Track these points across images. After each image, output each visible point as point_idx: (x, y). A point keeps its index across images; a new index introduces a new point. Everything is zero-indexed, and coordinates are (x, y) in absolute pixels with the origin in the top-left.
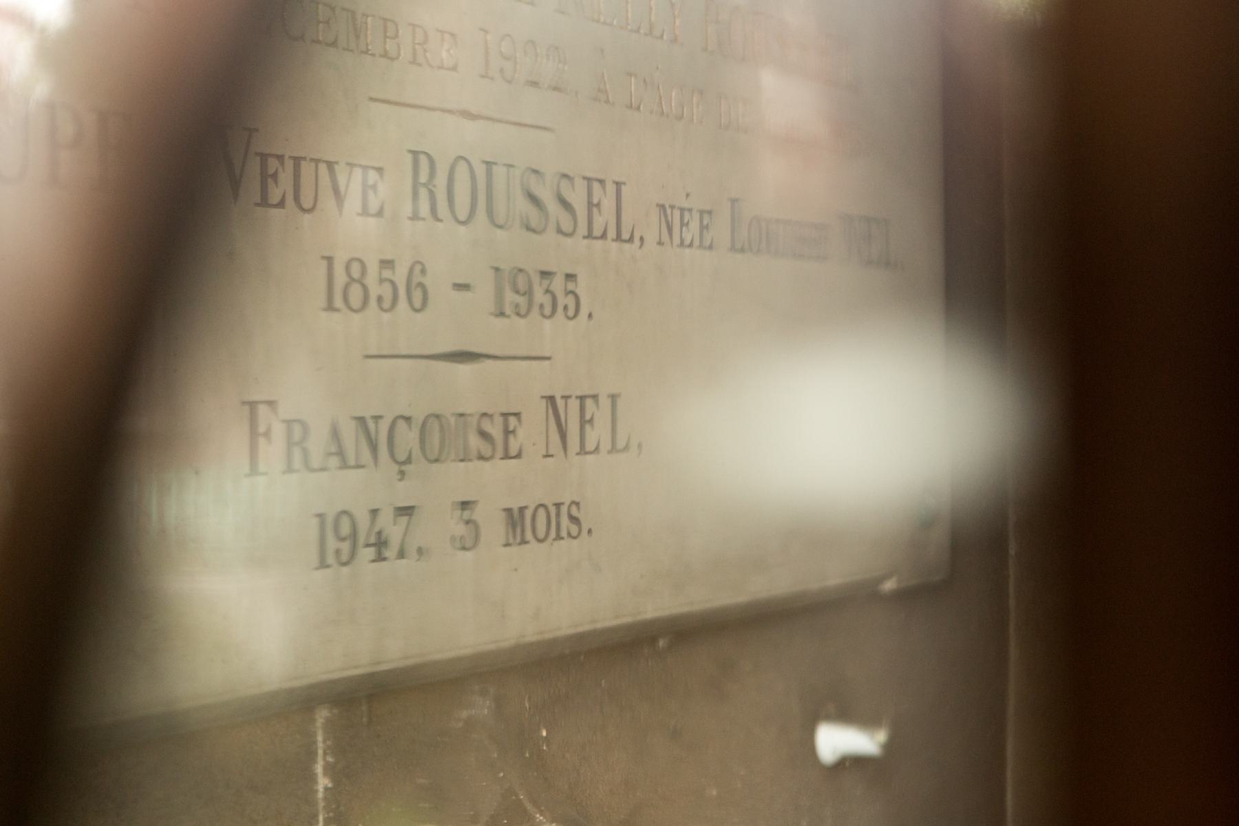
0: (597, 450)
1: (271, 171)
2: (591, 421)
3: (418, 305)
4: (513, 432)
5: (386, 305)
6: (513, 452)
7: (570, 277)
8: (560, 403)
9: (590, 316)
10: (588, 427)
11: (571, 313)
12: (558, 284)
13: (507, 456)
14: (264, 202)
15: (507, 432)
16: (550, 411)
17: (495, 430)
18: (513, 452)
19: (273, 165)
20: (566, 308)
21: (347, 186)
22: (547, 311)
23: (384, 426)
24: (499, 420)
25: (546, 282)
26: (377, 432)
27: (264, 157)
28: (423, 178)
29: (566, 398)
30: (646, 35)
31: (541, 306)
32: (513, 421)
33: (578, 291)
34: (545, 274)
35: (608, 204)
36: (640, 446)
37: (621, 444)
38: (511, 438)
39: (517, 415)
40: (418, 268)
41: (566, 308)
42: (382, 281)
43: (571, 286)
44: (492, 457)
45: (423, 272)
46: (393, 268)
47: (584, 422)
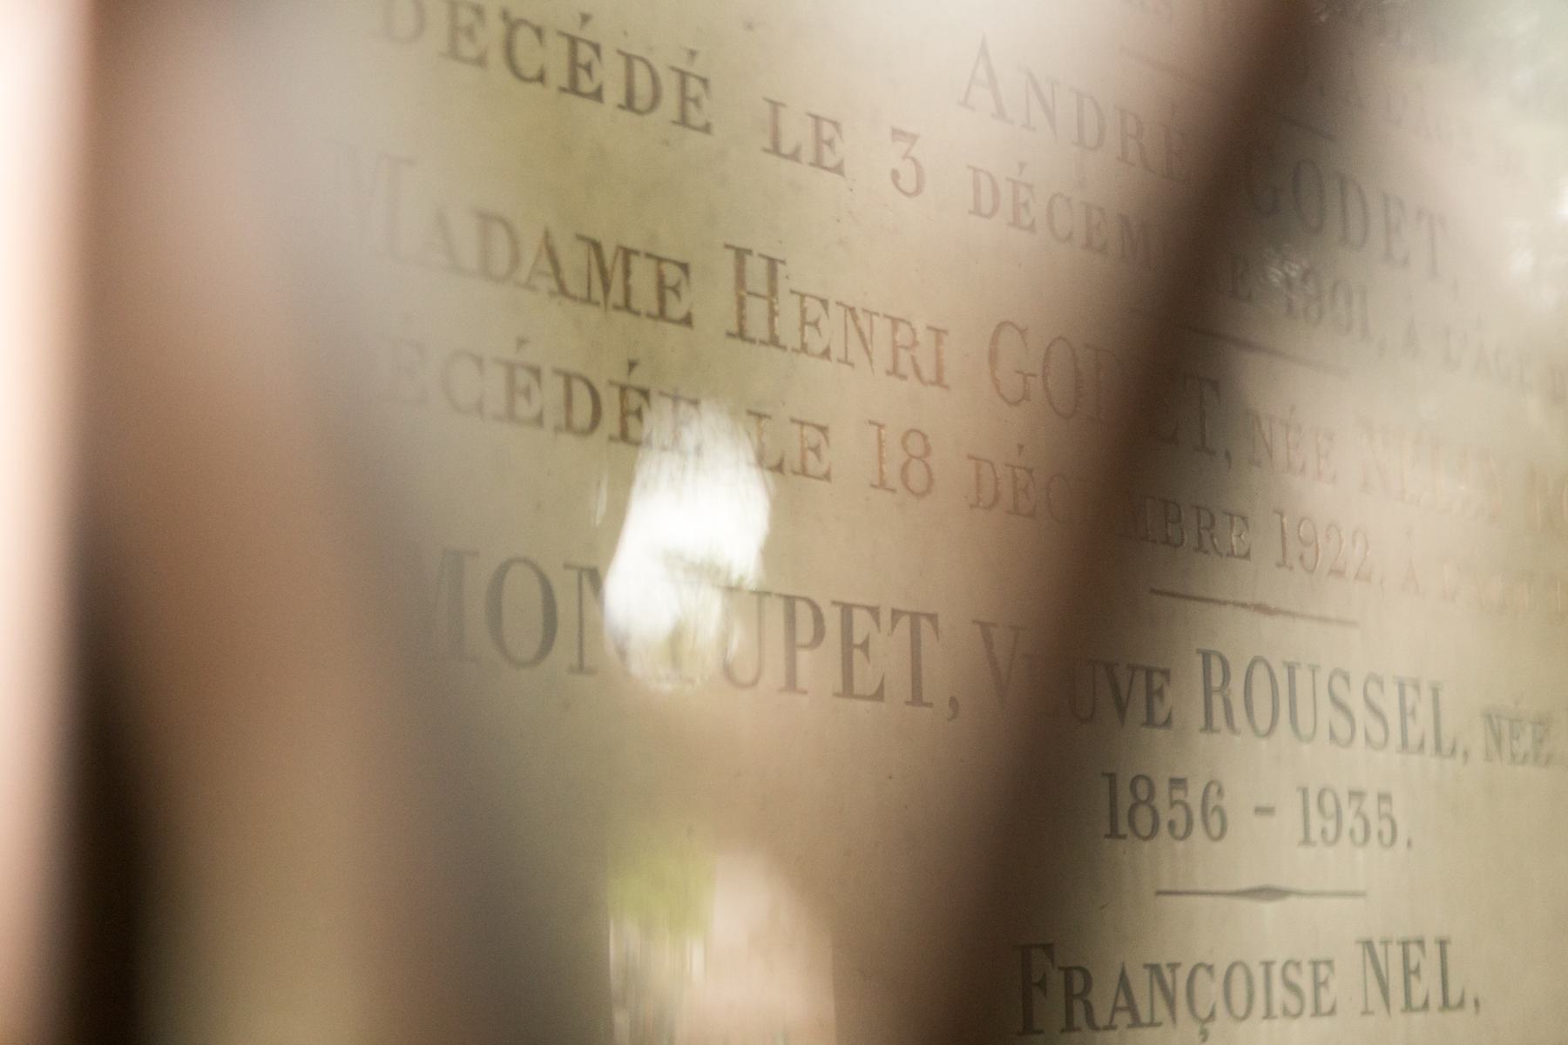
0: (1426, 1005)
1: (1156, 686)
2: (1417, 971)
3: (1216, 831)
4: (1325, 983)
5: (1180, 831)
6: (1325, 1007)
7: (1384, 797)
8: (1379, 949)
9: (1409, 844)
10: (1413, 979)
11: (1387, 837)
12: (1370, 805)
13: (1317, 1012)
14: (1150, 721)
15: (1318, 985)
16: (1368, 959)
17: (1305, 983)
18: (1325, 1007)
19: (1158, 680)
20: (1172, 825)
21: (1129, 692)
22: (1359, 836)
23: (1182, 975)
24: (1307, 969)
25: (1355, 804)
26: (1174, 984)
27: (1149, 672)
28: (1217, 682)
29: (1386, 943)
30: (557, 429)
31: (1352, 832)
32: (1323, 971)
33: (1188, 800)
34: (1357, 795)
35: (1424, 711)
36: (1477, 1003)
37: (1454, 998)
38: (1322, 990)
39: (1329, 963)
40: (1214, 789)
41: (1380, 834)
42: (1380, 817)
43: (1384, 807)
44: (1298, 1015)
45: (1220, 792)
46: (1185, 789)
47: (1409, 972)
